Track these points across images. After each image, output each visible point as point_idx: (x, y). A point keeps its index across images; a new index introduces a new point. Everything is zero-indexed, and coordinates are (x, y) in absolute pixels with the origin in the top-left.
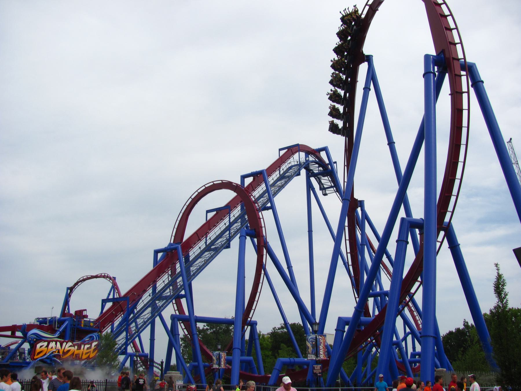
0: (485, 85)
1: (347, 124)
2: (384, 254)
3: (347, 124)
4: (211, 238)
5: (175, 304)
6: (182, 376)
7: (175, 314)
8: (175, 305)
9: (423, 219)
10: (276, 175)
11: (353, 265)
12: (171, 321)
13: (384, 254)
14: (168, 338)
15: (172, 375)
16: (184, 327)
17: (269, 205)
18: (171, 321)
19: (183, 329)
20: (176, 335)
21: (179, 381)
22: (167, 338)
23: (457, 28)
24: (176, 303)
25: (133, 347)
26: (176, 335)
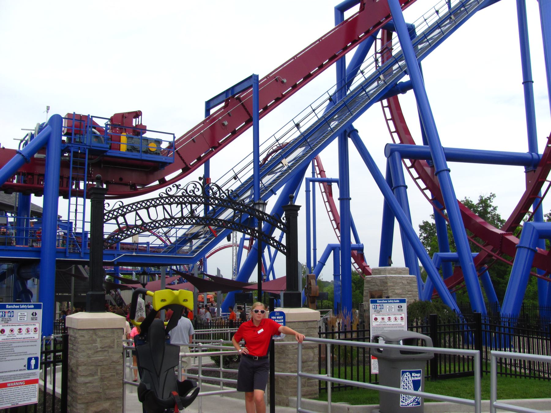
0: (280, 235)
1: (105, 196)
2: (252, 127)
3: (105, 196)
4: (239, 176)
5: (388, 109)
6: (408, 270)
7: (392, 142)
8: (387, 110)
9: (226, 238)
10: (425, 20)
11: (195, 132)
12: (386, 159)
13: (252, 127)
14: (382, 198)
15: (386, 277)
16: (416, 175)
17: (406, 79)
18: (385, 159)
19: (415, 180)
20: (398, 187)
21: (386, 306)
22: (379, 199)
23: (322, 193)
24: (389, 106)
25: (333, 220)
26: (398, 187)
